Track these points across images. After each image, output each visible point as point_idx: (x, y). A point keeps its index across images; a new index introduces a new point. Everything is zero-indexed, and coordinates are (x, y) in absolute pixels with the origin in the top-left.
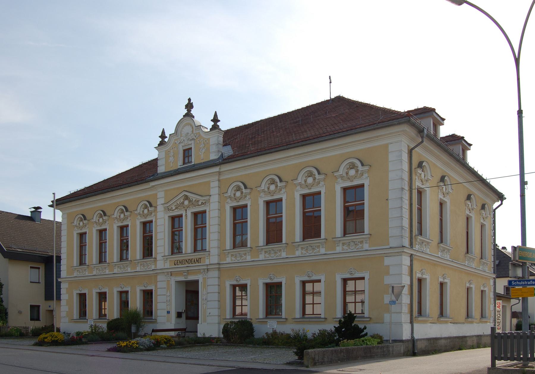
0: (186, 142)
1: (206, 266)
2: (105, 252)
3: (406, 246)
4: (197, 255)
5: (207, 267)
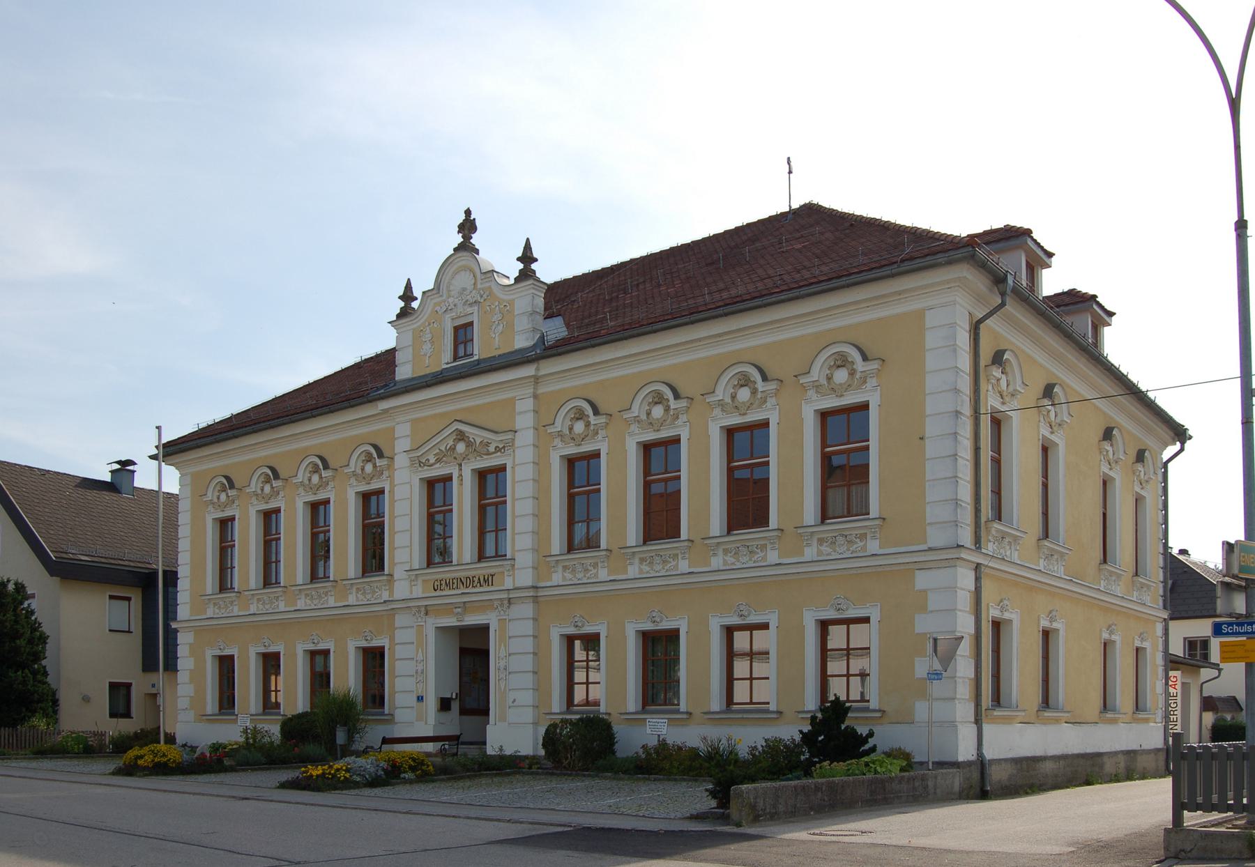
5: (509, 594)
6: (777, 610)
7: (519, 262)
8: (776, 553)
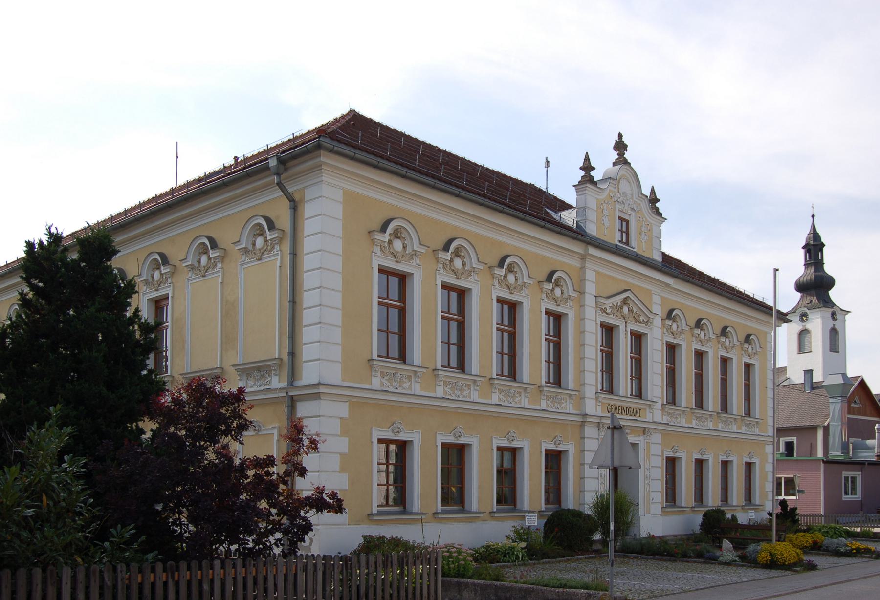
0: (626, 207)
1: (599, 418)
2: (501, 353)
3: (588, 414)
4: (635, 403)
5: (601, 420)
6: (420, 431)
7: (581, 171)
8: (527, 400)
